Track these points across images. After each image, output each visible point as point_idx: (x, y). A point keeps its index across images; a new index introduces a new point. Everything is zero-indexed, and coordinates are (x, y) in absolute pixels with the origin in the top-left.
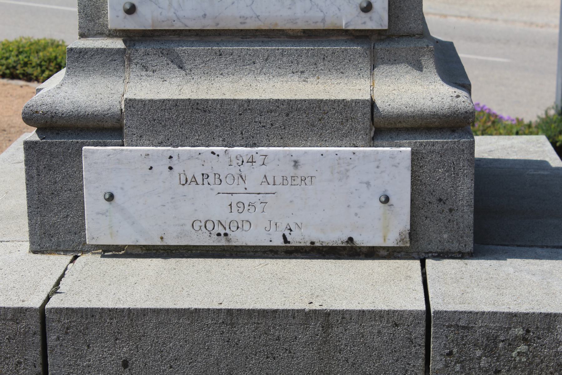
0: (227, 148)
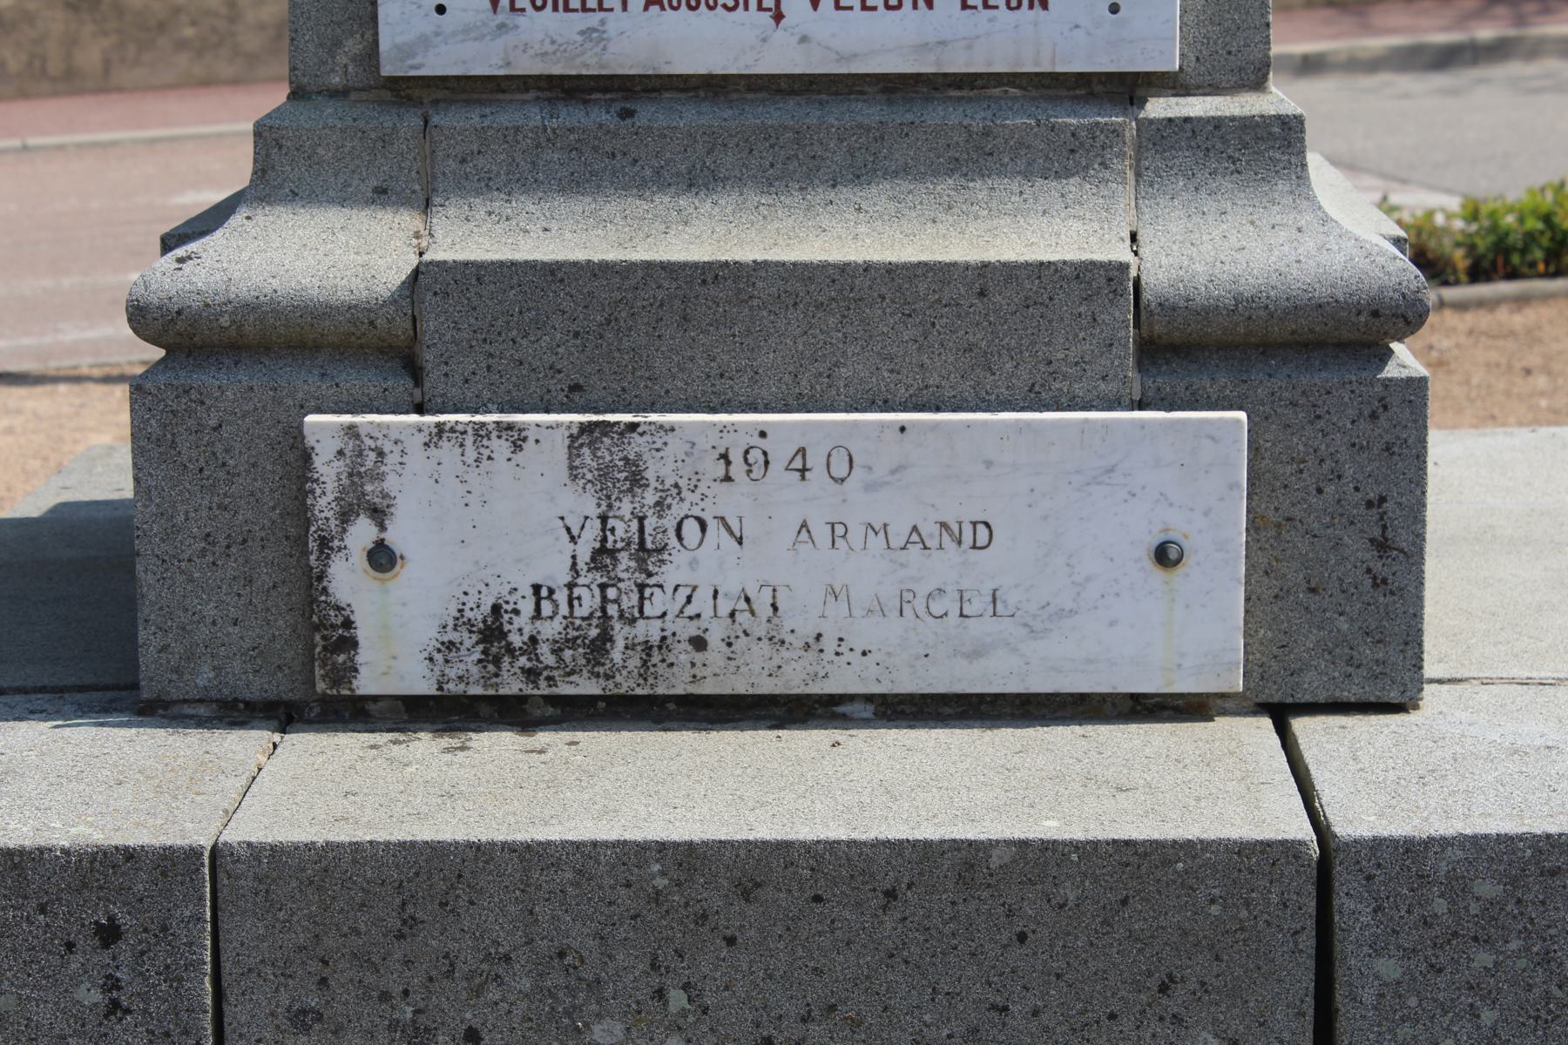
0: (347, 418)
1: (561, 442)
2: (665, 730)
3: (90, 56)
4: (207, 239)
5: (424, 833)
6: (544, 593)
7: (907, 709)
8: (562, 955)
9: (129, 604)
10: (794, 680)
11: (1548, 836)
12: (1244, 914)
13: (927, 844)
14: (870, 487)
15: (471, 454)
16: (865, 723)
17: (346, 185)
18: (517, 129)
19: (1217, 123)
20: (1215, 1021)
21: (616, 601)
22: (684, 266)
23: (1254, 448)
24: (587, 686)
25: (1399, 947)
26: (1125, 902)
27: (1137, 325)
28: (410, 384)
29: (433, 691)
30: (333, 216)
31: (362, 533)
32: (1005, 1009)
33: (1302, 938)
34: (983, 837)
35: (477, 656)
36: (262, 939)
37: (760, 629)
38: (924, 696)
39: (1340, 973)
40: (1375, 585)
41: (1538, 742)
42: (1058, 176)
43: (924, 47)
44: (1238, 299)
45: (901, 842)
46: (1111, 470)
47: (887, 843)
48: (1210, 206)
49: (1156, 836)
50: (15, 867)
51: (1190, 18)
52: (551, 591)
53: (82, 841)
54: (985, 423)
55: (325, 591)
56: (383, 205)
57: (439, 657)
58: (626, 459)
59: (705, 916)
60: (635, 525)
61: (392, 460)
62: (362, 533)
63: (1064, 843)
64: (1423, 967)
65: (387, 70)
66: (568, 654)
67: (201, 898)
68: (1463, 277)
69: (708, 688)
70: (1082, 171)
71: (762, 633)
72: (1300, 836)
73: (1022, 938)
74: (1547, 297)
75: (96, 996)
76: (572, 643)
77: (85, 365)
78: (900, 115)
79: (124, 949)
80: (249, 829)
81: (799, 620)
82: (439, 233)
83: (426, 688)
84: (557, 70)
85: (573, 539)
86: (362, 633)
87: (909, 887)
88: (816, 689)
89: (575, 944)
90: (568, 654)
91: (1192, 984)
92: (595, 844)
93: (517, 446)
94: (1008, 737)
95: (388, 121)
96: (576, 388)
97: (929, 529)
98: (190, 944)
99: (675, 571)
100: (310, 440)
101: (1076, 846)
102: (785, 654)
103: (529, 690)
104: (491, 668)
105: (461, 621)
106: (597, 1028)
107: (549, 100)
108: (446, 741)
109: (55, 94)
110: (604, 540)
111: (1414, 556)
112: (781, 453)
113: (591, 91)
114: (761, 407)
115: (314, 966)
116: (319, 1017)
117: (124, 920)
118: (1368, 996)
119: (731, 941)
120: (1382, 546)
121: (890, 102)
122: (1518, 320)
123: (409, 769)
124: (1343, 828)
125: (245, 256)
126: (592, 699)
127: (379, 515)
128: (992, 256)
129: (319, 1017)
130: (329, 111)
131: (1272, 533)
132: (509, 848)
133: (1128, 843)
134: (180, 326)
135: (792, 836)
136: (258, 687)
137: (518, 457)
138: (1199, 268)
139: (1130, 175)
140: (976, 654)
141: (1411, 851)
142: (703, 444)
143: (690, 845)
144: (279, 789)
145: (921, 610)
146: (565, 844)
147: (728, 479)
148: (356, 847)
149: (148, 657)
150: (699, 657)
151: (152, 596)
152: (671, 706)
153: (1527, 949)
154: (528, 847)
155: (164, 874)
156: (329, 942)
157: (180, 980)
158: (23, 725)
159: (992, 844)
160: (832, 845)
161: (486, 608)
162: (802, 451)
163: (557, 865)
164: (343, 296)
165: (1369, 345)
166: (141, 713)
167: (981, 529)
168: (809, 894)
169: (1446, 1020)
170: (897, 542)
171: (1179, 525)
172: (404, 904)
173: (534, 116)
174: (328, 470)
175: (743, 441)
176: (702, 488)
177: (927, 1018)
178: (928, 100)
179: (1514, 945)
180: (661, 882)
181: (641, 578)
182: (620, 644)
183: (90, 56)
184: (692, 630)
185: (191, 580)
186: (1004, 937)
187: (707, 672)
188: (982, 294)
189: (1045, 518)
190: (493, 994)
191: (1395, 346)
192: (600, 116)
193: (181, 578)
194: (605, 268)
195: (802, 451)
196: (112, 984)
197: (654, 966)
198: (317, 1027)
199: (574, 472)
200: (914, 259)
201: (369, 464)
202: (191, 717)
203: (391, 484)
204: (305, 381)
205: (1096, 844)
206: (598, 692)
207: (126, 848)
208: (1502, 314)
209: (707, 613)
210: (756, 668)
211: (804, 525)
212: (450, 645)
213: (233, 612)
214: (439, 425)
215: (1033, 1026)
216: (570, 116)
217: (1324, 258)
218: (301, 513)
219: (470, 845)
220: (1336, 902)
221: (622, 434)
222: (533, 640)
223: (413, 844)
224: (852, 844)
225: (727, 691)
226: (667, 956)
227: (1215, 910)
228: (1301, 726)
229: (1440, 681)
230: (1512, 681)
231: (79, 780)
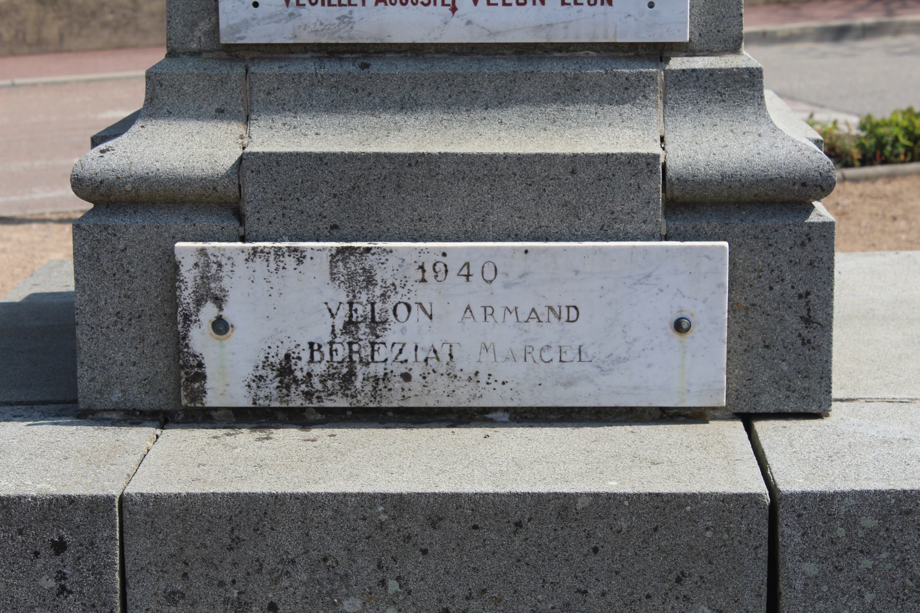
0: (200, 245)
1: (325, 259)
3: (52, 31)
6: (316, 347)
9: (72, 353)
10: (462, 399)
11: (905, 491)
13: (540, 496)
14: (507, 286)
15: (273, 266)
16: (504, 424)
17: (200, 107)
18: (300, 75)
19: (712, 72)
21: (358, 352)
22: (398, 155)
23: (733, 263)
24: (341, 402)
25: (817, 556)
26: (656, 529)
27: (664, 191)
28: (237, 224)
29: (250, 405)
30: (192, 126)
31: (209, 312)
32: (585, 592)
34: (573, 491)
35: (276, 384)
38: (538, 408)
39: (782, 571)
40: (803, 344)
41: (899, 436)
42: (618, 103)
43: (540, 27)
44: (723, 176)
45: (524, 494)
46: (649, 276)
47: (516, 495)
48: (707, 121)
49: (674, 491)
51: (696, 10)
52: (320, 346)
53: (43, 492)
54: (574, 248)
55: (187, 346)
56: (222, 120)
57: (254, 385)
58: (364, 269)
59: (409, 537)
60: (369, 307)
61: (226, 268)
62: (209, 312)
63: (620, 495)
65: (224, 40)
67: (114, 526)
68: (857, 163)
69: (412, 403)
70: (632, 100)
71: (444, 371)
72: (759, 491)
73: (596, 550)
74: (905, 175)
75: (52, 583)
76: (332, 377)
79: (68, 555)
80: (141, 486)
81: (465, 364)
82: (254, 136)
83: (246, 403)
84: (324, 40)
85: (333, 316)
86: (209, 371)
87: (529, 520)
88: (475, 404)
89: (333, 554)
91: (696, 578)
92: (345, 495)
93: (300, 261)
94: (588, 432)
95: (224, 70)
96: (334, 227)
97: (542, 310)
98: (107, 553)
99: (392, 334)
100: (178, 257)
101: (627, 496)
103: (307, 404)
104: (284, 391)
107: (319, 58)
108: (258, 434)
109: (31, 53)
110: (351, 316)
111: (826, 327)
112: (454, 267)
113: (344, 52)
114: (443, 238)
115: (180, 566)
116: (183, 596)
117: (68, 538)
118: (799, 585)
119: (424, 552)
120: (808, 321)
121: (519, 60)
122: (889, 188)
123: (238, 451)
124: (784, 486)
125: (140, 149)
126: (343, 410)
127: (219, 301)
128: (579, 150)
129: (183, 596)
130: (190, 64)
132: (295, 497)
133: (658, 495)
134: (102, 190)
135: (461, 490)
136: (147, 402)
137: (301, 267)
138: (701, 157)
139: (660, 103)
140: (569, 384)
141: (824, 499)
142: (409, 260)
143: (401, 496)
145: (537, 358)
146: (327, 495)
147: (423, 280)
148: (205, 496)
149: (83, 384)
150: (406, 385)
151: (85, 348)
152: (390, 414)
153: (892, 558)
154: (305, 496)
155: (91, 512)
157: (101, 574)
158: (10, 424)
159: (577, 496)
160: (484, 496)
161: (282, 356)
162: (467, 264)
163: (323, 507)
164: (198, 173)
165: (800, 203)
166: (78, 417)
167: (572, 310)
168: (471, 524)
169: (844, 600)
170: (523, 318)
172: (233, 530)
173: (311, 67)
174: (189, 275)
176: (408, 286)
177: (539, 597)
178: (541, 58)
179: (884, 555)
180: (384, 517)
181: (373, 338)
182: (360, 377)
183: (52, 31)
184: (403, 369)
185: (108, 339)
187: (411, 394)
188: (573, 172)
189: (610, 304)
190: (285, 582)
192: (349, 67)
193: (102, 338)
194: (352, 157)
195: (467, 264)
196: (61, 576)
197: (380, 566)
198: (182, 601)
201: (213, 271)
202: (108, 419)
203: (226, 283)
204: (176, 223)
205: (639, 495)
206: (347, 405)
207: (70, 497)
208: (880, 185)
209: (411, 359)
210: (440, 391)
211: (468, 308)
212: (261, 378)
213: (133, 359)
214: (255, 250)
216: (332, 67)
217: (774, 151)
218: (173, 300)
220: (780, 530)
221: (361, 254)
222: (309, 375)
223: (238, 494)
225: (423, 405)
226: (387, 560)
227: (709, 534)
229: (841, 400)
230: (883, 400)
231: (42, 456)
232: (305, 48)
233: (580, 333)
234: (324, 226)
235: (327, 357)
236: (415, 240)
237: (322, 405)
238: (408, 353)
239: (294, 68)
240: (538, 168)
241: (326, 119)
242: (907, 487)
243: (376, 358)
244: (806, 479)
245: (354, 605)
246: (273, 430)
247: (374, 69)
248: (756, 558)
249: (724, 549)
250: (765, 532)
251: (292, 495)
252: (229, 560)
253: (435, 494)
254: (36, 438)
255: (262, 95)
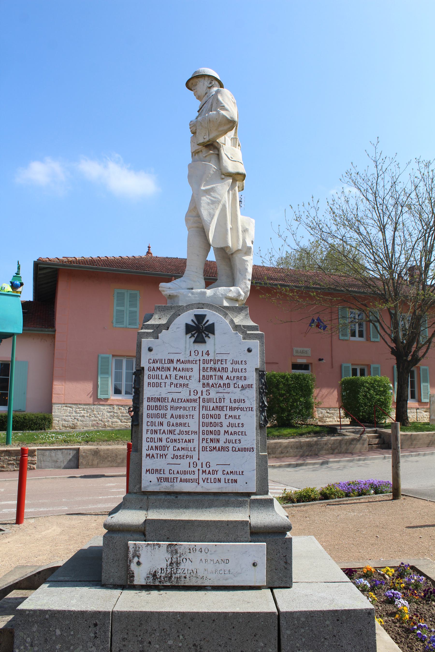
0: (134, 542)
1: (165, 547)
2: (180, 591)
3: (95, 462)
4: (115, 514)
5: (144, 610)
6: (162, 569)
7: (216, 588)
8: (164, 630)
9: (101, 566)
10: (199, 583)
11: (312, 611)
12: (267, 624)
13: (219, 613)
14: (211, 554)
15: (152, 548)
16: (210, 590)
17: (136, 506)
18: (161, 499)
19: (261, 500)
20: (263, 641)
21: (173, 571)
22: (184, 520)
23: (267, 548)
24: (168, 584)
25: (290, 629)
26: (249, 622)
27: (250, 530)
28: (144, 537)
29: (145, 584)
30: (134, 511)
31: (136, 560)
32: (231, 639)
33: (276, 627)
34: (228, 611)
35: (152, 579)
36: (118, 626)
37: (194, 575)
38: (219, 586)
39: (281, 633)
40: (285, 569)
41: (310, 594)
42: (238, 507)
43: (219, 488)
44: (265, 526)
45: (215, 612)
46: (246, 552)
47: (213, 612)
48: (260, 512)
49: (254, 611)
50: (82, 614)
51: (257, 484)
52: (163, 569)
53: (92, 610)
54: (228, 544)
55: (130, 568)
56: (141, 510)
57: (146, 579)
58: (175, 549)
59: (186, 624)
60: (176, 559)
61: (141, 549)
62: (136, 560)
63: (240, 612)
64: (294, 632)
65: (142, 490)
66: (166, 579)
67: (110, 619)
68: (296, 502)
69: (186, 584)
70: (242, 506)
71: (195, 576)
72: (275, 611)
73: (234, 627)
74: (308, 505)
75: (93, 635)
76: (166, 577)
77: (92, 512)
78: (216, 498)
79: (98, 627)
80: (117, 608)
81: (200, 574)
82: (149, 514)
83: (144, 583)
84: (167, 491)
85: (167, 561)
86: (135, 575)
87: (217, 619)
88: (202, 585)
89: (166, 628)
90: (166, 579)
91: (259, 635)
92: (169, 612)
93: (159, 547)
94: (231, 593)
95: (142, 497)
96: (168, 538)
97: (220, 560)
98: (108, 627)
99: (182, 566)
100: (129, 545)
101: (242, 613)
102: (198, 579)
103: (160, 584)
104: (154, 581)
105: (150, 573)
106: (169, 642)
107: (166, 495)
108: (147, 592)
109: (90, 468)
110: (172, 561)
111: (291, 564)
112: (198, 549)
113: (171, 493)
114: (195, 541)
115: (126, 631)
116: (127, 639)
117: (98, 623)
118: (286, 637)
119: (189, 628)
120: (286, 563)
121: (214, 496)
122: (304, 509)
123: (142, 598)
124: (281, 610)
125: (121, 517)
126: (169, 586)
127: (138, 557)
128: (229, 519)
129: (127, 639)
130: (134, 496)
131: (270, 561)
132: (157, 612)
133: (249, 612)
134: (111, 527)
135: (199, 611)
136: (119, 582)
137: (159, 549)
138: (259, 521)
139: (249, 507)
140: (226, 579)
141: (291, 614)
142: (187, 547)
143: (184, 612)
144: (122, 601)
145: (218, 573)
146: (165, 612)
147: (190, 552)
148: (133, 612)
149: (103, 577)
150: (185, 580)
151: (104, 568)
152: (181, 587)
153: (309, 629)
154: (159, 612)
155: (104, 615)
156: (129, 627)
157: (106, 633)
158: (84, 588)
159: (229, 613)
160: (205, 613)
161: (154, 571)
162: (201, 548)
163: (164, 615)
164: (135, 524)
165: (283, 533)
166: (102, 586)
167: (227, 560)
168: (201, 620)
169: (297, 640)
170: (215, 562)
171: (257, 560)
172: (140, 621)
173: (163, 497)
174: (131, 550)
175: (193, 547)
176: (186, 554)
177: (219, 640)
178: (220, 496)
179: (307, 628)
180: (179, 618)
181: (177, 567)
182: (173, 577)
183: (95, 462)
184: (184, 575)
185: (110, 566)
186: (231, 627)
187: (186, 582)
188: (228, 525)
189: (237, 559)
190: (153, 636)
191: (287, 533)
192: (173, 497)
193: (109, 565)
194: (173, 520)
195: (201, 548)
196: (96, 633)
197: (178, 632)
198: (126, 641)
199: (167, 551)
200: (218, 520)
201: (137, 549)
202: (109, 587)
203: (140, 552)
204: (128, 536)
205: (245, 613)
206: (170, 585)
207: (99, 611)
208: (302, 508)
209: (187, 573)
210: (193, 581)
211: (201, 560)
212: (148, 577)
213: (116, 571)
214: (148, 544)
215: (235, 642)
216: (168, 497)
217: (277, 520)
218: (127, 556)
219: (150, 612)
220: (280, 622)
221: (175, 545)
222: (161, 576)
223: (142, 611)
224: (208, 612)
225: (189, 585)
226: (180, 630)
227: (262, 623)
228: (275, 590)
229: (295, 582)
230: (305, 582)
231: (92, 598)
232: (162, 492)
233: (229, 566)
234: (165, 538)
235: (165, 572)
236: (188, 542)
237: (163, 584)
238: (186, 571)
239: (159, 497)
240: (219, 524)
241: (167, 510)
242: (312, 610)
243: (178, 572)
244: (287, 607)
245: (171, 643)
246: (151, 591)
247: (179, 498)
248: (275, 629)
249: (266, 627)
250: (277, 622)
251: (156, 612)
252: (139, 629)
253: (192, 612)
254: (91, 592)
255: (151, 504)
